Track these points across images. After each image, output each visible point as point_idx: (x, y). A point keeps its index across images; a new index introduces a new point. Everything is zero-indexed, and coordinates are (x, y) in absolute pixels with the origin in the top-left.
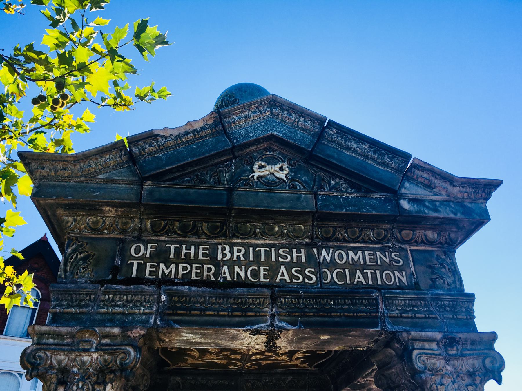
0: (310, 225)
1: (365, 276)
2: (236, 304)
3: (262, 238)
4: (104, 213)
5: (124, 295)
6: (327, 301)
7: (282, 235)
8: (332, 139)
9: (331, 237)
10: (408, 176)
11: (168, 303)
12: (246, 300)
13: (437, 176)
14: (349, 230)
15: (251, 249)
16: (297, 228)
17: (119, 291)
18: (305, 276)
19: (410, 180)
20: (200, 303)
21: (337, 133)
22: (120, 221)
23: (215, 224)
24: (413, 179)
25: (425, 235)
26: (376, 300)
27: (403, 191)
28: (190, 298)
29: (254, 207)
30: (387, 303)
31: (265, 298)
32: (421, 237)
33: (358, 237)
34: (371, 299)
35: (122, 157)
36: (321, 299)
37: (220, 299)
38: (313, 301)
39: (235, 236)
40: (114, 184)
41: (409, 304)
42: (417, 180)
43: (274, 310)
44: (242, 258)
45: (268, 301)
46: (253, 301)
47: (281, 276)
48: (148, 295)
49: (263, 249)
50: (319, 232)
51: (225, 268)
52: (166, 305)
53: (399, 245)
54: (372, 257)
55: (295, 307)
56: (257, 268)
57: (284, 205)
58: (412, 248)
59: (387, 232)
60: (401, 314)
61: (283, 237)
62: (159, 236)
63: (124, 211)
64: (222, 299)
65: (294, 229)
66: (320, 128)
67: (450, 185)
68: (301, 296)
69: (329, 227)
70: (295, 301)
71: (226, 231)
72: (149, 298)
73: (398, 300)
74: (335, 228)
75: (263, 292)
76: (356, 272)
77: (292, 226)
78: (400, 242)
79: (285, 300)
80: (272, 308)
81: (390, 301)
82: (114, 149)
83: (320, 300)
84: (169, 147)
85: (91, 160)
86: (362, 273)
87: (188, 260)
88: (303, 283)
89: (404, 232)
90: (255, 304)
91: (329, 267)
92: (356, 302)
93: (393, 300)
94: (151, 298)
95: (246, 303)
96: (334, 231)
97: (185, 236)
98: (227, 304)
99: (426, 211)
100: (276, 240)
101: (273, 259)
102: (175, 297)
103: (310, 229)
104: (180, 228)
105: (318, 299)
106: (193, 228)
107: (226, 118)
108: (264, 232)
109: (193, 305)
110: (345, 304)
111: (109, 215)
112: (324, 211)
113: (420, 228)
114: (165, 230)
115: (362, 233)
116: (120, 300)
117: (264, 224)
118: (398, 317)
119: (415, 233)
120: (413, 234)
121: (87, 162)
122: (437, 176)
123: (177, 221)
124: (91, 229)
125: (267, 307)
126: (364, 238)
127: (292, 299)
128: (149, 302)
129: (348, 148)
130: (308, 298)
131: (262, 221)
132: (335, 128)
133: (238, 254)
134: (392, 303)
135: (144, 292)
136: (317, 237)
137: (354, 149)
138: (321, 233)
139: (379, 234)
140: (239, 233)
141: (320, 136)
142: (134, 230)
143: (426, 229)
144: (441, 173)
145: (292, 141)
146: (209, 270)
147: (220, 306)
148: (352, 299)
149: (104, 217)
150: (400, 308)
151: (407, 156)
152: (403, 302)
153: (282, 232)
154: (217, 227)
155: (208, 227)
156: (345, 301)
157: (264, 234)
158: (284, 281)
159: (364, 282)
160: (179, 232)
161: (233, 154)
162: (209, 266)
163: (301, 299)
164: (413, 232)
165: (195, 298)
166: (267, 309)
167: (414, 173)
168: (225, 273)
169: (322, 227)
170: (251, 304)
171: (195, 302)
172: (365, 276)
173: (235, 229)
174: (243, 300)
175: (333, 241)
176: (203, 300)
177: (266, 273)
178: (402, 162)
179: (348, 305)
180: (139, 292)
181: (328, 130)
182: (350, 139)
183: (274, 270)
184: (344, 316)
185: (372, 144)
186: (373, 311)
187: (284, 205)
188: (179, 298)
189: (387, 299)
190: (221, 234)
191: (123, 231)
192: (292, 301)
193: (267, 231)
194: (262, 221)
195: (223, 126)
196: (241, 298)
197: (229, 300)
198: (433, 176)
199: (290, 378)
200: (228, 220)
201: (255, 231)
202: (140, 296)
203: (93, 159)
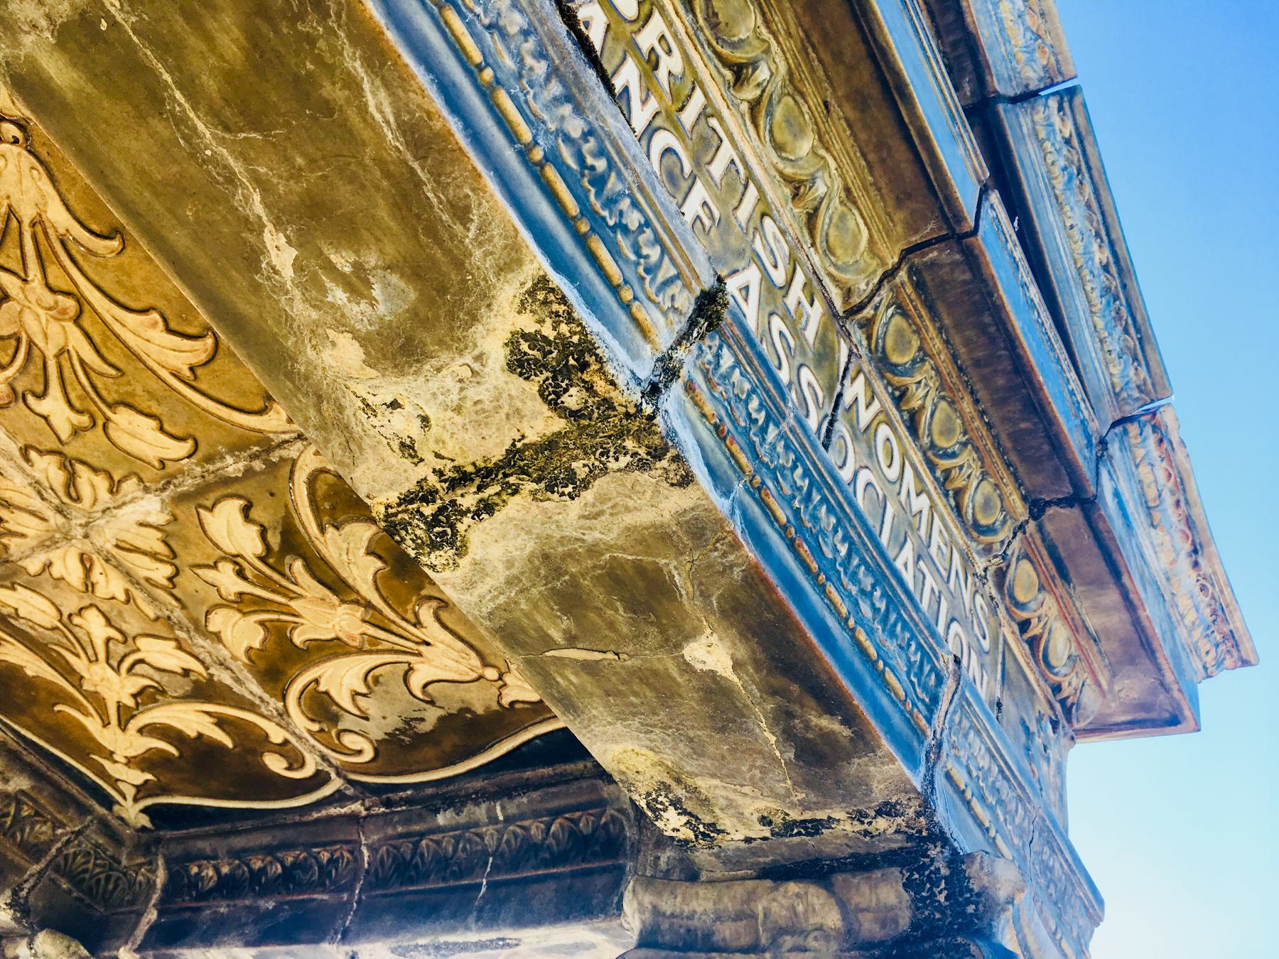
0: (883, 263)
3: (743, 116)
10: (1126, 432)
13: (1182, 504)
21: (1068, 142)
26: (940, 681)
59: (1004, 522)
66: (1041, 80)
69: (917, 332)
75: (692, 249)
103: (875, 272)
117: (793, 84)
119: (1040, 596)
125: (665, 314)
126: (954, 473)
134: (966, 736)
136: (867, 325)
148: (892, 601)
163: (777, 425)
178: (1138, 387)
185: (1117, 262)
198: (1172, 493)
199: (20, 783)
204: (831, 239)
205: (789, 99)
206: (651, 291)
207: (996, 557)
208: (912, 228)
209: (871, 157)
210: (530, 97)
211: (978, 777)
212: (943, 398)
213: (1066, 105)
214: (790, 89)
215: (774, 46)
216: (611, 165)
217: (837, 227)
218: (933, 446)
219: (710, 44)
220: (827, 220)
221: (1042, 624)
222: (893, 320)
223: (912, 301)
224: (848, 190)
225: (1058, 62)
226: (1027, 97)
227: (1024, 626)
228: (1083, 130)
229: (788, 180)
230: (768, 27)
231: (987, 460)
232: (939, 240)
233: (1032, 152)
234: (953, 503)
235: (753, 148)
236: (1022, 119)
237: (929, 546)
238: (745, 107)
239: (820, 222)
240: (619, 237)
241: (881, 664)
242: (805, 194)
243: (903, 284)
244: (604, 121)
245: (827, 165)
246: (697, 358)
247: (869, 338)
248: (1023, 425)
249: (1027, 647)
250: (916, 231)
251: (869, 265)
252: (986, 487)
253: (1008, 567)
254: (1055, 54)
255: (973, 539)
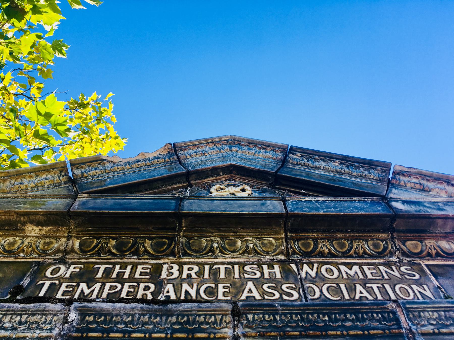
0: (282, 238)
1: (370, 291)
2: (180, 323)
3: (221, 256)
4: (25, 233)
5: (17, 315)
6: (319, 317)
7: (246, 251)
8: (297, 162)
9: (312, 252)
10: (393, 184)
11: (78, 325)
12: (195, 318)
13: (429, 178)
14: (334, 242)
15: (207, 267)
16: (266, 242)
17: (12, 310)
18: (282, 293)
19: (397, 187)
20: (125, 323)
21: (302, 156)
22: (43, 241)
23: (160, 240)
24: (400, 186)
25: (439, 247)
26: (394, 313)
27: (391, 195)
28: (112, 318)
29: (208, 211)
30: (411, 316)
31: (223, 315)
32: (434, 248)
33: (349, 250)
34: (385, 312)
35: (61, 178)
36: (308, 314)
37: (156, 318)
38: (296, 316)
39: (186, 254)
40: (43, 198)
41: (446, 317)
42: (406, 186)
43: (237, 330)
44: (194, 276)
45: (228, 319)
46: (205, 318)
47: (248, 293)
48: (51, 314)
49: (222, 268)
50: (297, 246)
51: (170, 287)
52: (74, 326)
53: (408, 259)
54: (374, 271)
55: (270, 325)
56: (213, 286)
57: (245, 209)
58: (427, 262)
59: (387, 243)
60: (438, 329)
61: (249, 253)
62: (88, 258)
63: (50, 230)
64: (159, 318)
65: (263, 243)
66: (283, 155)
67: (448, 185)
68: (278, 310)
69: (307, 239)
70: (269, 317)
71: (174, 247)
72: (52, 318)
73: (428, 311)
74: (315, 241)
75: (221, 307)
76: (355, 286)
77: (259, 239)
78: (407, 256)
79: (254, 317)
80: (235, 327)
81: (416, 314)
82: (53, 169)
83: (308, 316)
84: (117, 171)
85: (24, 178)
86: (365, 288)
87: (120, 279)
88: (280, 300)
89: (408, 243)
90: (208, 323)
91: (315, 282)
92: (362, 316)
93: (419, 312)
94: (55, 319)
95: (194, 322)
96: (315, 244)
97: (121, 257)
98: (165, 323)
99: (428, 210)
100: (240, 257)
101: (237, 276)
102: (89, 316)
103: (282, 242)
104: (115, 247)
105: (304, 314)
106: (133, 246)
107: (181, 150)
108: (225, 248)
109: (115, 326)
110: (346, 320)
111: (30, 235)
112: (296, 212)
113: (429, 238)
114: (96, 249)
115: (352, 245)
116: (10, 322)
117: (223, 238)
118: (434, 334)
119: (424, 244)
120: (423, 246)
121: (19, 180)
122: (429, 178)
123: (113, 239)
124: (5, 251)
125: (226, 327)
127: (264, 315)
128: (50, 323)
129: (316, 168)
130: (288, 313)
131: (220, 235)
132: (299, 152)
133: (189, 272)
134: (420, 316)
135: (47, 311)
136: (294, 253)
137: (324, 168)
138: (298, 246)
139: (376, 246)
140: (191, 250)
141: (284, 161)
142: (58, 251)
143: (437, 238)
144: (432, 174)
145: (253, 167)
146: (147, 288)
147: (155, 326)
148: (356, 312)
149: (24, 237)
150: (434, 323)
151: (386, 166)
152: (436, 315)
153: (247, 246)
154: (164, 243)
155: (151, 245)
156: (346, 316)
157: (223, 250)
158: (253, 298)
159: (370, 297)
160: (114, 251)
161: (189, 183)
162: (147, 284)
164: (421, 242)
165: (119, 317)
166: (226, 330)
167: (399, 179)
168: (168, 292)
169: (298, 240)
170: (202, 323)
171: (118, 323)
172: (370, 291)
173: (186, 245)
174: (191, 318)
175: (316, 257)
176: (130, 319)
177: (227, 290)
178: (382, 172)
179: (352, 321)
180: (40, 311)
181: (291, 155)
182: (317, 160)
183: (237, 287)
184: (348, 335)
186: (393, 327)
187: (245, 209)
188: (95, 317)
189: (410, 311)
190: (169, 251)
191: (44, 253)
192: (264, 317)
193: (227, 247)
194: (220, 235)
195: (178, 157)
196: (188, 316)
197: (170, 319)
198: (423, 179)
200: (177, 235)
201: (212, 246)
202: (39, 316)
203: (27, 177)
204: (265, 250)
205: (227, 241)
206: (219, 327)
207: (395, 252)
208: (279, 225)
209: (254, 227)
210: (160, 327)
211: (437, 322)
212: (333, 241)
213: (293, 152)
214: (225, 239)
215: (213, 238)
216: (188, 316)
217: (263, 247)
218: (343, 253)
219: (201, 255)
220: (260, 248)
221: (433, 250)
222: (299, 244)
223: (298, 236)
224: (257, 238)
225: (282, 148)
226: (284, 161)
227: (429, 255)
228: (301, 151)
229: (243, 253)
230: (208, 237)
231: (362, 238)
232: (286, 220)
233: (297, 168)
234: (367, 256)
235: (230, 258)
236: (288, 166)
237: (367, 277)
238: (220, 254)
239: (259, 251)
240: (201, 326)
241: (366, 332)
242: (249, 251)
243: (291, 236)
244: (179, 310)
245: (248, 240)
246: (242, 326)
247: (298, 254)
248: (357, 222)
249: (438, 258)
250: (281, 225)
251: (279, 243)
252: (370, 243)
253: (402, 250)
254: (280, 148)
255: (384, 257)
